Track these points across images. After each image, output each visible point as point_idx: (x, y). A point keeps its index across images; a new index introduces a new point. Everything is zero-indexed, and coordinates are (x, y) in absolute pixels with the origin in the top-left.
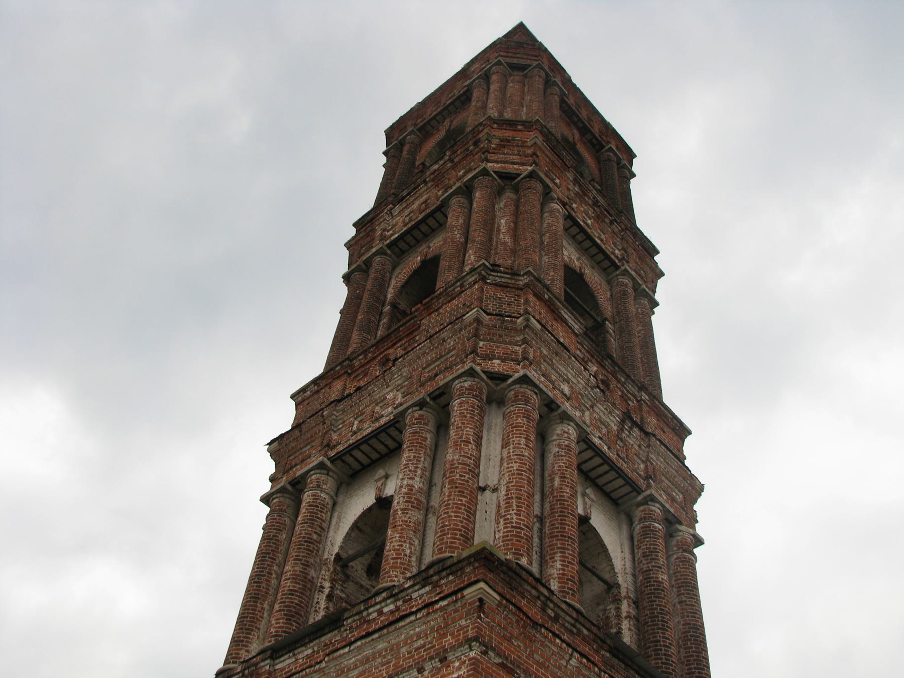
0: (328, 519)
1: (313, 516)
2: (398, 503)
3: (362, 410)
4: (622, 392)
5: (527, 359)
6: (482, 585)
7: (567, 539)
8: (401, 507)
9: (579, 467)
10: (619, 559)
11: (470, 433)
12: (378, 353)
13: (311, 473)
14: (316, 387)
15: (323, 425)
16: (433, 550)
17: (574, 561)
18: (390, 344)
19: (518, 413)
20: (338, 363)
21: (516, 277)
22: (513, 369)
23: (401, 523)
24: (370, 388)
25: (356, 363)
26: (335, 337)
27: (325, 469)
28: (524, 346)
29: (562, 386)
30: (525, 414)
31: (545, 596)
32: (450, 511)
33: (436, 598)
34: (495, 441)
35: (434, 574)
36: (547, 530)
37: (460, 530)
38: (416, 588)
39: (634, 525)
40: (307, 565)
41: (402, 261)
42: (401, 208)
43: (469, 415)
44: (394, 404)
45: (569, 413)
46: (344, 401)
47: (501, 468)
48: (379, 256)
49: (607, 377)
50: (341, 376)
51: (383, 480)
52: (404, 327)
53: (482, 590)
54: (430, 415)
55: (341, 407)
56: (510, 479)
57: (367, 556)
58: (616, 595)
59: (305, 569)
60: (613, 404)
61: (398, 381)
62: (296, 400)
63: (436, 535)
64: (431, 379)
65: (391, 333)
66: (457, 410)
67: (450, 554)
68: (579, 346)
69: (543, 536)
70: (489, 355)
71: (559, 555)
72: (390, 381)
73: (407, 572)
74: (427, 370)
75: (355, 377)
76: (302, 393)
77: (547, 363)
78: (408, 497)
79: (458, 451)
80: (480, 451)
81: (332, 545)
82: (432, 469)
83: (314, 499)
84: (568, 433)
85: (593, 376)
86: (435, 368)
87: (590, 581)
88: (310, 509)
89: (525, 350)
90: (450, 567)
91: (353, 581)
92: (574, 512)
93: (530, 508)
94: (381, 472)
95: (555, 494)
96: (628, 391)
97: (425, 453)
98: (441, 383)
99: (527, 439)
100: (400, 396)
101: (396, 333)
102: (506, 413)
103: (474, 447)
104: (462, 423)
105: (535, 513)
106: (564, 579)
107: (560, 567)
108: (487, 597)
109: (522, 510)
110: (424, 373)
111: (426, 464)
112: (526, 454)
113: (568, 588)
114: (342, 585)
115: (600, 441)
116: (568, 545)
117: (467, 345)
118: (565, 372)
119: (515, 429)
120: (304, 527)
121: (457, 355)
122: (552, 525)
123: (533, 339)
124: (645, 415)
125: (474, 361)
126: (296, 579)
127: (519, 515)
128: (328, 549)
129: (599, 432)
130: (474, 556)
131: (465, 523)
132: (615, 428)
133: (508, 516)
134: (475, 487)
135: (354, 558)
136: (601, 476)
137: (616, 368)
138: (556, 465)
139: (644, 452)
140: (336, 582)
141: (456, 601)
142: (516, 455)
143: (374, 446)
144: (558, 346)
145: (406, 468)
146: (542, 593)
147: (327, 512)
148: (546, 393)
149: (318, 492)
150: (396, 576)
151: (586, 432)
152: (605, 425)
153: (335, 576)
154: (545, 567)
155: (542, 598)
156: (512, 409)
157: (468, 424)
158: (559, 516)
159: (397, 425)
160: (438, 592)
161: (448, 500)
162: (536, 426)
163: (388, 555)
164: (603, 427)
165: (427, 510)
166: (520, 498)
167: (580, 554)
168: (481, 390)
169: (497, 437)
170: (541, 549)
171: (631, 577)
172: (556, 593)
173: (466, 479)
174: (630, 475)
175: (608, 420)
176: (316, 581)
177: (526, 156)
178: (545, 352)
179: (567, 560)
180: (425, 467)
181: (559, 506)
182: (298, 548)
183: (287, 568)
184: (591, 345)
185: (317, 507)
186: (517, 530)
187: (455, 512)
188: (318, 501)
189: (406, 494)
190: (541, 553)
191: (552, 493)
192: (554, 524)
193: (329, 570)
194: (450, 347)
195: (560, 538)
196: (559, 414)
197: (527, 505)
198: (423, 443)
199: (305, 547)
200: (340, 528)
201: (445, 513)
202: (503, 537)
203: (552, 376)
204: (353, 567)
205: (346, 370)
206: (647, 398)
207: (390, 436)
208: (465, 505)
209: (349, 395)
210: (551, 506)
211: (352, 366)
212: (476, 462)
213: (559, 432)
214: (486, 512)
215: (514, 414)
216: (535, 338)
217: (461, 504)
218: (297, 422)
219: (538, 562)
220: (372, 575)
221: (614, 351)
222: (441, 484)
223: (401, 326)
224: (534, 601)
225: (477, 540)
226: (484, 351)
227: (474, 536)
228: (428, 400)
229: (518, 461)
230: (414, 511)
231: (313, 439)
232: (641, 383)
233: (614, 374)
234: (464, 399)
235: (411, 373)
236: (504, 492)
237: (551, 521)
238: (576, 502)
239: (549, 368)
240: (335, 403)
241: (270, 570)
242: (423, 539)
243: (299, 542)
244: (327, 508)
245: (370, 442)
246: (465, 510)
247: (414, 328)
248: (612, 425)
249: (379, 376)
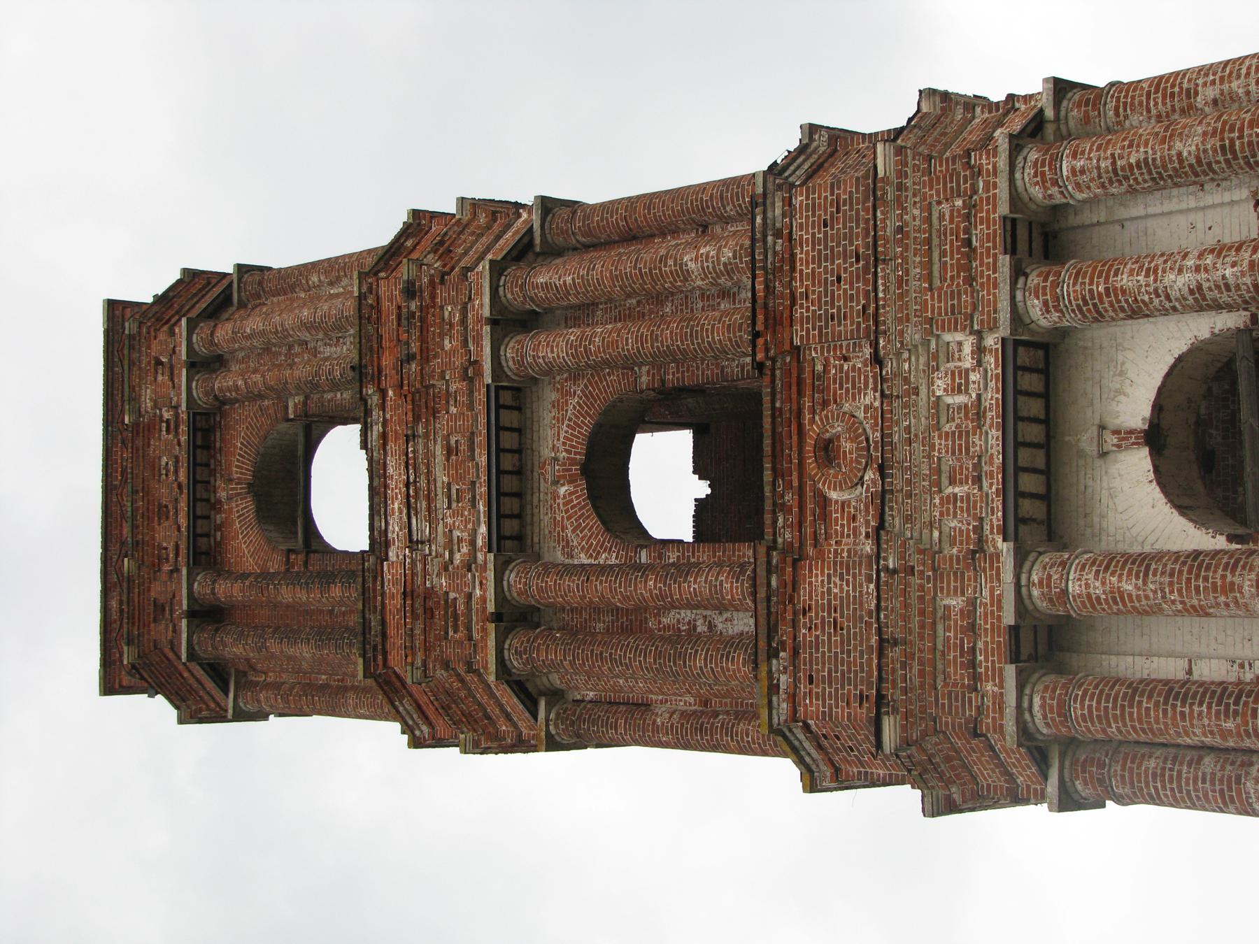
14: (782, 654)
18: (795, 438)
21: (809, 151)
41: (536, 548)
42: (424, 513)
48: (507, 572)
52: (778, 396)
55: (895, 522)
74: (937, 283)
76: (775, 699)
177: (489, 227)
223: (773, 402)
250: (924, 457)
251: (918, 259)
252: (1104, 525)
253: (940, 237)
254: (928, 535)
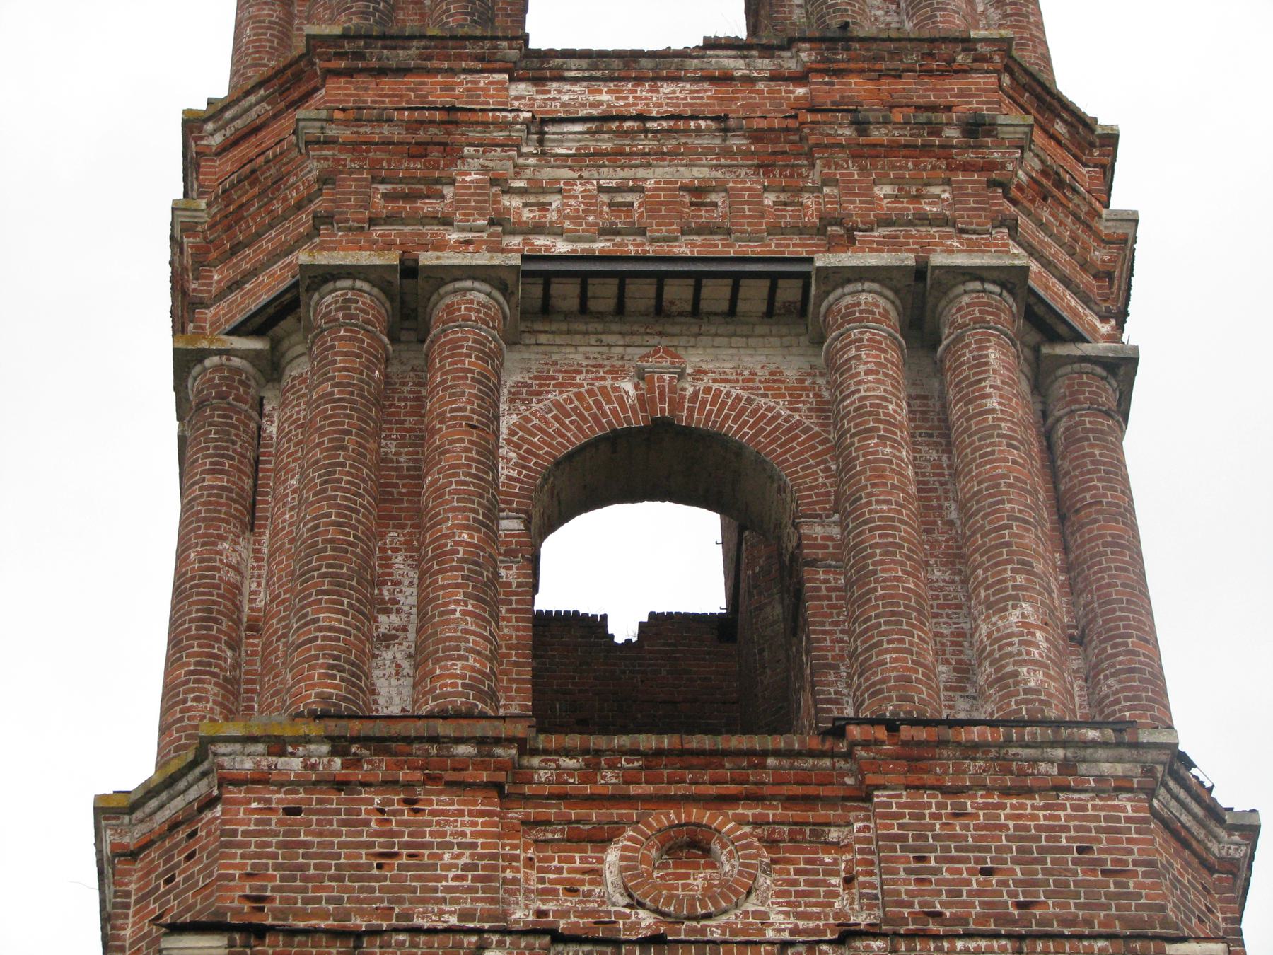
12: (649, 789)
18: (713, 790)
21: (1212, 825)
41: (528, 339)
42: (592, 145)
48: (487, 288)
52: (786, 762)
76: (260, 748)
211: (521, 775)
223: (776, 753)
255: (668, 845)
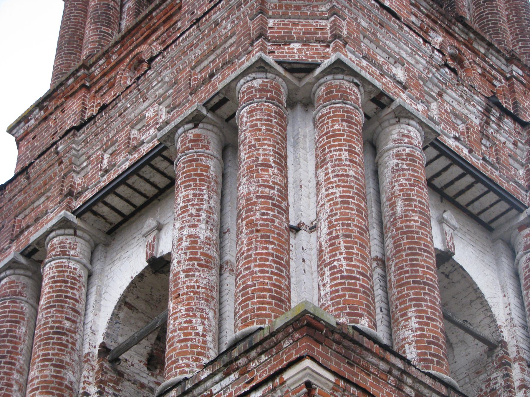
0: (84, 297)
1: (61, 296)
2: (178, 262)
3: (113, 137)
4: (483, 68)
5: (340, 37)
6: (307, 363)
7: (422, 285)
8: (184, 267)
9: (430, 183)
10: (502, 306)
11: (268, 152)
12: (125, 52)
13: (52, 235)
14: (42, 112)
15: (59, 165)
16: (235, 323)
17: (435, 315)
18: (141, 38)
19: (334, 116)
20: (69, 73)
22: (320, 54)
23: (186, 290)
24: (119, 105)
25: (96, 71)
26: (61, 36)
27: (70, 227)
28: (332, 19)
29: (394, 70)
30: (344, 116)
31: (399, 369)
32: (252, 265)
33: (246, 389)
34: (306, 160)
35: (240, 355)
36: (392, 276)
37: (270, 291)
38: (217, 378)
39: (518, 256)
40: (60, 366)
43: (264, 127)
44: (157, 123)
45: (408, 107)
46: (85, 128)
47: (317, 197)
49: (458, 50)
50: (77, 91)
51: (154, 234)
52: (158, 11)
53: (308, 371)
54: (210, 133)
55: (81, 136)
56: (332, 211)
57: (144, 342)
58: (503, 357)
59: (59, 372)
60: (471, 88)
61: (157, 90)
62: (17, 135)
63: (236, 301)
64: (204, 82)
65: (141, 22)
66: (247, 122)
67: (259, 326)
68: (414, 10)
69: (388, 285)
70: (284, 37)
71: (413, 309)
72: (147, 92)
73: (202, 357)
74: (198, 70)
75: (96, 92)
76: (23, 124)
77: (369, 39)
78: (192, 253)
79: (255, 180)
80: (286, 177)
81: (94, 333)
82: (222, 210)
83: (60, 272)
84: (408, 136)
85: (439, 51)
86: (208, 66)
87: (463, 342)
88: (56, 287)
89: (335, 24)
90: (260, 343)
91: (129, 380)
92: (428, 247)
93: (364, 248)
94: (150, 223)
95: (399, 225)
96: (491, 66)
97: (208, 187)
98: (220, 86)
99: (351, 151)
100: (164, 111)
101: (147, 21)
102: (317, 118)
103: (276, 171)
104: (256, 140)
105: (374, 254)
106: (423, 342)
107: (417, 326)
108: (316, 379)
109: (353, 253)
110: (195, 74)
111: (212, 204)
112: (352, 173)
113: (431, 354)
114: (113, 387)
115: (457, 143)
116: (425, 294)
117: (251, 26)
118: (396, 49)
119: (332, 139)
120: (50, 312)
121: (238, 43)
122: (399, 268)
123: (345, 7)
124: (520, 98)
125: (263, 49)
126: (47, 387)
127: (351, 260)
128: (88, 340)
129: (455, 130)
130: (292, 324)
131: (276, 280)
132: (477, 121)
133: (335, 263)
134: (283, 227)
135: (126, 347)
136: (462, 192)
137: (471, 35)
138: (397, 184)
139: (522, 151)
140: (105, 384)
141: (274, 390)
142: (338, 176)
143: (136, 186)
144: (381, 13)
145: (184, 212)
146: (394, 366)
147: (80, 287)
148: (370, 83)
149: (64, 261)
150: (188, 366)
151: (435, 132)
152: (461, 120)
153: (102, 375)
154: (396, 328)
155: (396, 372)
156: (325, 111)
157: (264, 139)
158: (407, 255)
159: (165, 153)
160: (247, 380)
161: (249, 250)
162: (361, 132)
163: (173, 338)
164: (459, 122)
165: (221, 267)
166: (349, 236)
167: (443, 305)
168: (277, 89)
169: (308, 154)
170: (388, 304)
171: (522, 330)
172: (415, 363)
173: (270, 217)
174: (505, 186)
175: (465, 112)
176: (76, 387)
178: (364, 24)
179: (425, 315)
180: (211, 208)
181: (405, 241)
182: (45, 344)
183: (32, 374)
184: (432, 6)
185: (65, 282)
186: (350, 281)
187: (259, 266)
188: (66, 274)
189: (188, 248)
190: (388, 310)
191: (394, 225)
192: (402, 267)
193: (93, 369)
194: (226, 33)
195: (412, 285)
196: (393, 111)
197: (360, 245)
198: (205, 174)
199: (55, 341)
200: (102, 308)
201: (246, 269)
202: (331, 293)
203: (378, 57)
204: (126, 360)
205: (83, 82)
206: (521, 72)
207: (158, 170)
208: (272, 255)
209: (92, 118)
210: (395, 242)
211: (90, 76)
212: (282, 193)
213: (395, 136)
214: (304, 261)
215: (329, 118)
216: (348, 5)
217: (268, 254)
218: (21, 166)
219: (385, 323)
220: (156, 368)
221: (466, 10)
222: (235, 228)
223: (154, 9)
224: (384, 378)
225: (295, 301)
226: (276, 33)
227: (289, 295)
228: (204, 112)
229: (340, 183)
230: (203, 271)
231: (47, 187)
232: (509, 53)
233: (468, 45)
234: (255, 105)
235: (175, 77)
236: (325, 231)
237: (397, 264)
238: (429, 233)
239: (372, 46)
240: (73, 131)
241: (9, 380)
242: (220, 310)
243: (45, 334)
244: (79, 282)
245: (130, 181)
246: (273, 261)
247: (173, 11)
248: (472, 117)
249: (130, 86)
250: (117, 129)
251: (205, 48)
252: (116, 262)
253: (222, 52)
254: (83, 160)
255: (132, 68)
